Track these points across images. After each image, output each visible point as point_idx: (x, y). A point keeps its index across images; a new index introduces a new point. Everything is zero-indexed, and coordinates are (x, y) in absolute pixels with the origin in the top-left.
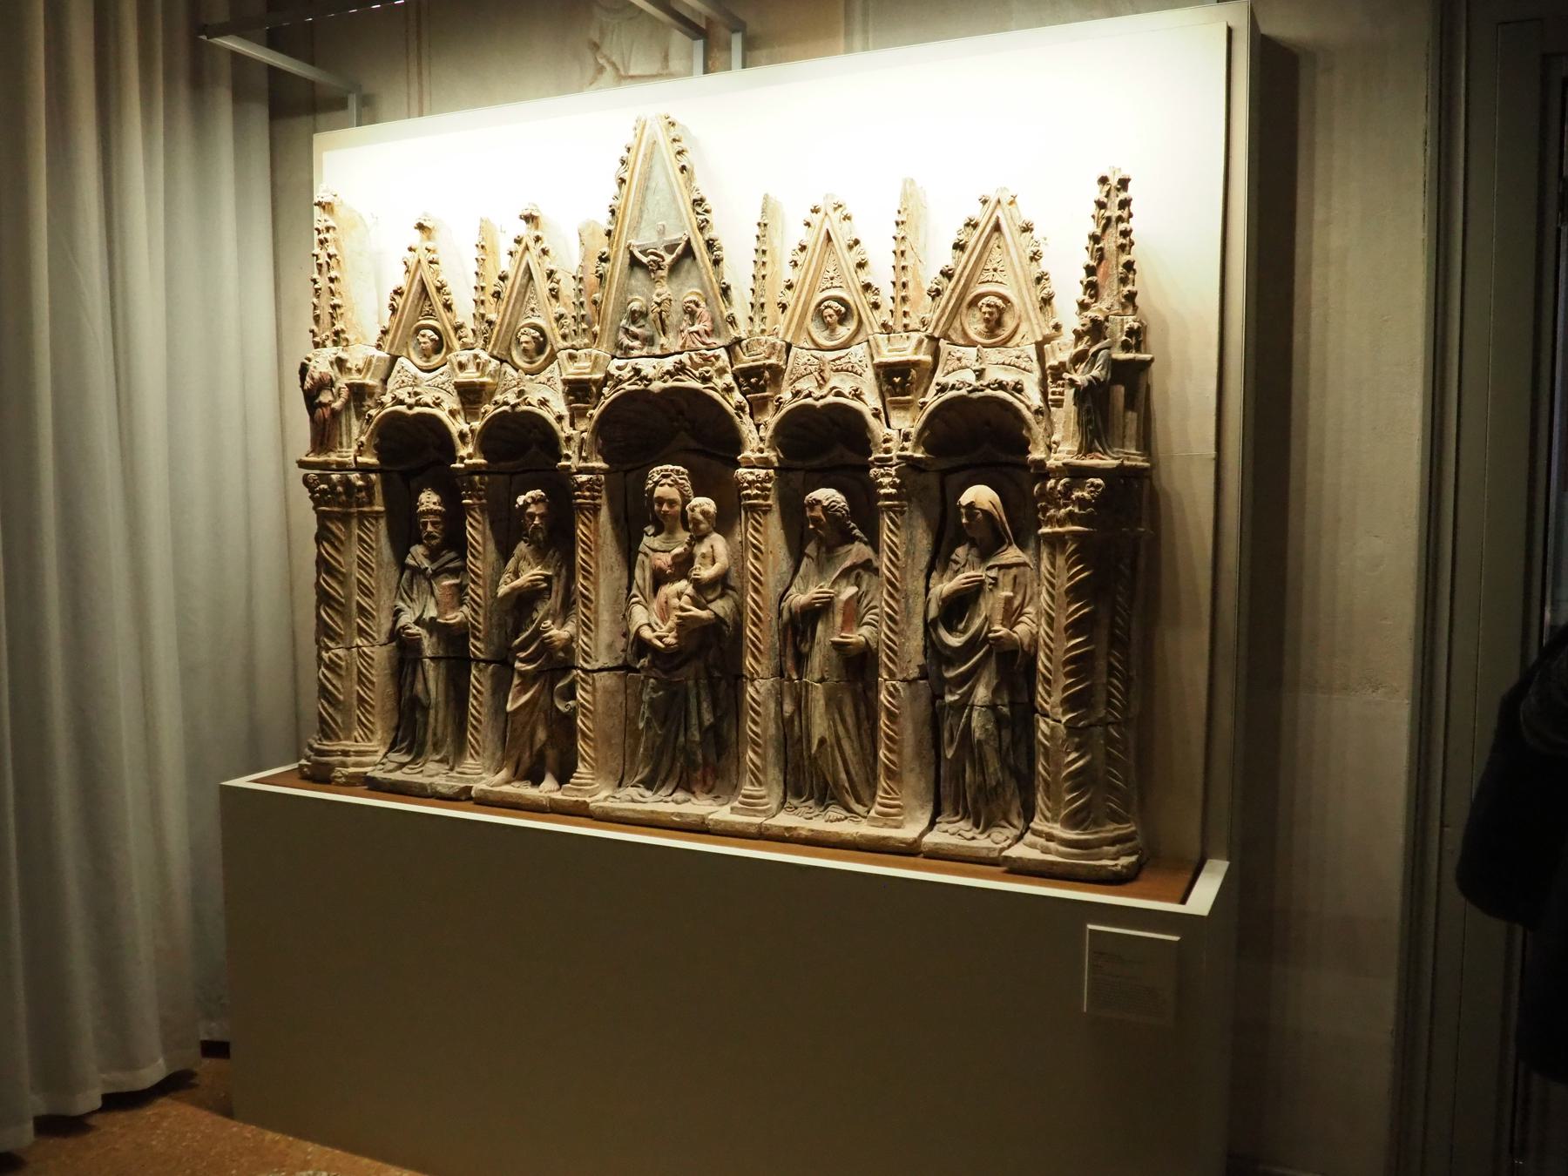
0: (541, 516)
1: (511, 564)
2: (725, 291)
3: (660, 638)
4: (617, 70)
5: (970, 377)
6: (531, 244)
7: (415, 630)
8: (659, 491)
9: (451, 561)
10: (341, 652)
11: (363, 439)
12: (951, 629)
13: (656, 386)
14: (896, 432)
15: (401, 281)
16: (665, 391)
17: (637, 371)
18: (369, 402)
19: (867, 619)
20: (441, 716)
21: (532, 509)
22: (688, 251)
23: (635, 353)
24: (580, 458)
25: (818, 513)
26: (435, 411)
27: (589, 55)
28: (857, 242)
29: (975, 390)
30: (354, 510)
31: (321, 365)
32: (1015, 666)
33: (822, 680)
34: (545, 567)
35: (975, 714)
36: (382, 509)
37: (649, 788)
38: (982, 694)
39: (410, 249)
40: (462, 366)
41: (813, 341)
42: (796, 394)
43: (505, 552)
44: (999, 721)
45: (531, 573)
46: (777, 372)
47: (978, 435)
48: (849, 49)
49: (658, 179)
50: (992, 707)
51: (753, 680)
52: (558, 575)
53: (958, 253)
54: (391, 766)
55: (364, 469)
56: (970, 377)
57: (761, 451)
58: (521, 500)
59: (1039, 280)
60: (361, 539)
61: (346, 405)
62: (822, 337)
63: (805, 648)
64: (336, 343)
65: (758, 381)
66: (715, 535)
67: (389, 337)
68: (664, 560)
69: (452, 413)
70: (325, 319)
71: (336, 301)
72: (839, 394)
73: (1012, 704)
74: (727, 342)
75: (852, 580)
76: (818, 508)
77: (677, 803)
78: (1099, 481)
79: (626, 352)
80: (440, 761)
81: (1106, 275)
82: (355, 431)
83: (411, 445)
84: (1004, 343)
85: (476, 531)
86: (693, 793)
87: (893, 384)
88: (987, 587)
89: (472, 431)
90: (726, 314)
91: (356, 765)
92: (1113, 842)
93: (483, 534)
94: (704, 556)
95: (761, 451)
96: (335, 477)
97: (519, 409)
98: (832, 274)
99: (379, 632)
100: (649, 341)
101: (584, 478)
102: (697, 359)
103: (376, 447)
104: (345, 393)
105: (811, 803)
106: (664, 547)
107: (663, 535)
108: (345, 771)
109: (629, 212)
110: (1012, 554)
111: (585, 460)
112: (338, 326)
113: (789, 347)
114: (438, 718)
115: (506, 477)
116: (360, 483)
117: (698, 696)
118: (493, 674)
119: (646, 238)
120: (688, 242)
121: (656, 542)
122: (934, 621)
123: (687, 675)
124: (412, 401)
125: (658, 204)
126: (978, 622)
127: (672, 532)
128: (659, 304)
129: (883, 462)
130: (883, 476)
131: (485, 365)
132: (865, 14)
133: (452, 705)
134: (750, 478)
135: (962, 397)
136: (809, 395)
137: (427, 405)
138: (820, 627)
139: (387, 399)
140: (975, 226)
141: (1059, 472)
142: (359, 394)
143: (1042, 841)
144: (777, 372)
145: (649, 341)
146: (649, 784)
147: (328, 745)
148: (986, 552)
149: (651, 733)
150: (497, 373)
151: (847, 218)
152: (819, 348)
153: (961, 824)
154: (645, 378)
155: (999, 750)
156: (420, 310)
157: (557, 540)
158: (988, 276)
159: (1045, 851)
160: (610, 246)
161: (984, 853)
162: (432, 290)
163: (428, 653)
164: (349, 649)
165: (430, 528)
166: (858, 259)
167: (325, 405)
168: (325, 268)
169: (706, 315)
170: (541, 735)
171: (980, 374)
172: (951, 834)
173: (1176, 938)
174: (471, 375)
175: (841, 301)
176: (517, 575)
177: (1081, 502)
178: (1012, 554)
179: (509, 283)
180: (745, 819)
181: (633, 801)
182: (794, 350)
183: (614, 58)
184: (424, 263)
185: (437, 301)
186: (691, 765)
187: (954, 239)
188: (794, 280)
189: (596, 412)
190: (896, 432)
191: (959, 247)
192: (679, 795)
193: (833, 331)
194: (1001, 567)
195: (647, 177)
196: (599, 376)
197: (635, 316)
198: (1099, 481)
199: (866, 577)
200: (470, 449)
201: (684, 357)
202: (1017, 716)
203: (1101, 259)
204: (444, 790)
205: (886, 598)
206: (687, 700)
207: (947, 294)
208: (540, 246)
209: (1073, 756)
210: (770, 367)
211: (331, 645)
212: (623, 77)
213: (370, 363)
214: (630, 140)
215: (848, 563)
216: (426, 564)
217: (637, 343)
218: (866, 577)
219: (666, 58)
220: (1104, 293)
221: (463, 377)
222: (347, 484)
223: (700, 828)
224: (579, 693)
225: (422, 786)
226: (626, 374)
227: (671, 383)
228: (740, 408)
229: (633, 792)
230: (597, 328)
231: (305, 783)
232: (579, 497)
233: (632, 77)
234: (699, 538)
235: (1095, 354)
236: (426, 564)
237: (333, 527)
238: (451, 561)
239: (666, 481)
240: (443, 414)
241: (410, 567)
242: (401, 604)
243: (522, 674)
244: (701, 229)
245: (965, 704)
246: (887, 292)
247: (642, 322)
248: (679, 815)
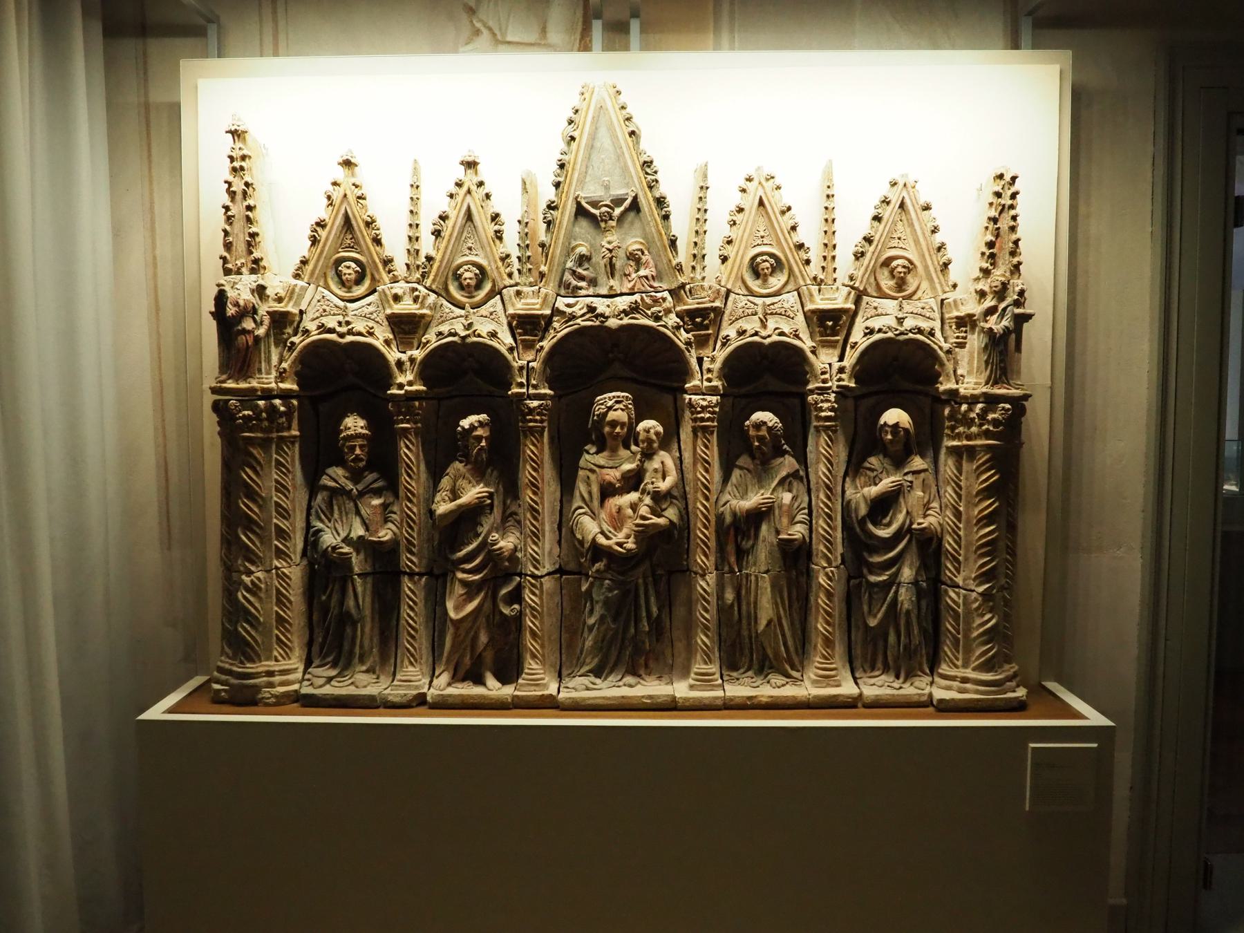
0: (486, 438)
1: (445, 482)
2: (673, 243)
3: (620, 545)
4: (494, 35)
5: (894, 323)
6: (474, 188)
7: (346, 549)
8: (612, 415)
9: (375, 481)
10: (259, 574)
11: (284, 365)
12: (875, 524)
13: (613, 323)
14: (830, 366)
15: (323, 213)
16: (622, 328)
17: (591, 309)
18: (290, 330)
19: (797, 519)
20: (367, 629)
21: (480, 432)
22: (635, 206)
23: (583, 292)
24: (531, 386)
25: (764, 432)
26: (369, 340)
27: (464, 17)
28: (789, 209)
29: (902, 333)
30: (274, 435)
31: (241, 290)
32: (928, 547)
33: (767, 572)
34: (486, 485)
35: (902, 590)
36: (297, 433)
37: (598, 676)
38: (907, 573)
39: (335, 184)
40: (397, 298)
41: (747, 288)
42: (741, 333)
43: (436, 473)
44: (920, 593)
45: (472, 493)
46: (719, 312)
47: (901, 368)
48: (717, 47)
49: (604, 140)
50: (915, 583)
51: (703, 576)
52: (497, 491)
53: (876, 223)
54: (322, 681)
55: (285, 396)
56: (894, 323)
57: (709, 380)
58: (465, 423)
59: (939, 249)
60: (279, 463)
61: (267, 334)
62: (755, 285)
63: (746, 544)
64: (253, 271)
65: (704, 321)
66: (662, 453)
67: (309, 268)
68: (613, 475)
69: (387, 342)
70: (240, 246)
71: (254, 229)
72: (479, 336)
73: (927, 580)
74: (674, 286)
75: (786, 487)
76: (764, 428)
77: (631, 686)
78: (1008, 406)
79: (574, 292)
80: (367, 671)
81: (1001, 249)
82: (275, 359)
83: (338, 373)
84: (910, 297)
85: (409, 452)
86: (640, 676)
87: (826, 327)
88: (906, 489)
89: (412, 360)
90: (674, 263)
91: (282, 684)
92: (1009, 679)
93: (417, 457)
94: (656, 471)
95: (709, 380)
96: (261, 403)
97: (469, 340)
98: (762, 233)
99: (295, 553)
100: (593, 282)
101: (535, 403)
102: (648, 300)
103: (297, 374)
104: (267, 320)
105: (750, 673)
106: (611, 463)
107: (605, 454)
108: (273, 691)
109: (578, 167)
110: (918, 463)
111: (535, 387)
112: (256, 254)
113: (729, 292)
114: (367, 632)
115: (435, 402)
116: (282, 409)
117: (646, 585)
118: (426, 584)
119: (590, 191)
120: (635, 198)
121: (601, 459)
122: (864, 518)
123: (638, 576)
124: (344, 329)
125: (604, 162)
126: (901, 517)
127: (614, 451)
128: (610, 251)
129: (822, 391)
130: (822, 401)
131: (425, 298)
132: (732, 13)
133: (377, 617)
134: (705, 403)
135: (890, 339)
136: (756, 334)
137: (360, 334)
138: (764, 527)
139: (312, 326)
140: (888, 203)
141: (972, 400)
142: (280, 321)
143: (955, 684)
144: (719, 312)
145: (593, 282)
146: (598, 672)
147: (251, 668)
148: (899, 462)
149: (603, 628)
150: (434, 307)
151: (778, 188)
152: (752, 293)
153: (883, 677)
154: (602, 315)
155: (918, 617)
156: (346, 245)
157: (500, 460)
158: (895, 243)
159: (961, 691)
160: (557, 195)
161: (916, 698)
162: (358, 224)
163: (357, 570)
164: (268, 571)
165: (358, 451)
166: (791, 223)
167: (249, 332)
168: (239, 197)
169: (652, 263)
170: (483, 638)
171: (900, 321)
172: (877, 686)
173: (1095, 745)
174: (406, 307)
175: (772, 255)
176: (455, 495)
177: (995, 422)
178: (918, 463)
179: (450, 223)
180: (690, 694)
181: (588, 689)
182: (732, 296)
183: (491, 23)
184: (351, 198)
185: (366, 236)
186: (638, 650)
187: (873, 212)
188: (733, 237)
189: (547, 344)
190: (830, 366)
191: (877, 218)
192: (629, 679)
193: (765, 281)
194: (914, 473)
195: (593, 137)
196: (548, 312)
197: (583, 260)
198: (1008, 406)
199: (795, 484)
200: (410, 377)
201: (637, 297)
202: (932, 588)
203: (997, 236)
204: (397, 700)
205: (803, 500)
206: (637, 596)
207: (868, 255)
208: (483, 191)
209: (988, 616)
210: (714, 309)
211: (253, 568)
212: (499, 42)
213: (293, 292)
214: (576, 101)
215: (784, 473)
216: (350, 486)
217: (583, 284)
218: (795, 484)
219: (544, 31)
220: (1000, 262)
221: (398, 308)
222: (272, 410)
223: (671, 706)
224: (527, 596)
225: (372, 698)
226: (578, 310)
227: (626, 321)
228: (688, 343)
229: (585, 681)
230: (544, 268)
231: (217, 707)
232: (531, 421)
233: (509, 43)
234: (648, 455)
235: (1004, 310)
236: (350, 486)
237: (255, 452)
238: (375, 481)
239: (614, 405)
240: (379, 344)
241: (326, 488)
242: (320, 525)
243: (464, 583)
244: (650, 188)
245: (893, 581)
246: (815, 254)
247: (586, 266)
248: (650, 697)
